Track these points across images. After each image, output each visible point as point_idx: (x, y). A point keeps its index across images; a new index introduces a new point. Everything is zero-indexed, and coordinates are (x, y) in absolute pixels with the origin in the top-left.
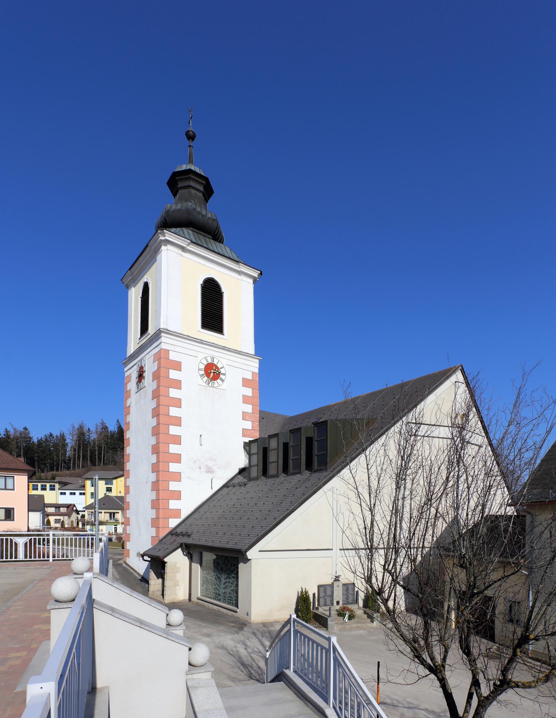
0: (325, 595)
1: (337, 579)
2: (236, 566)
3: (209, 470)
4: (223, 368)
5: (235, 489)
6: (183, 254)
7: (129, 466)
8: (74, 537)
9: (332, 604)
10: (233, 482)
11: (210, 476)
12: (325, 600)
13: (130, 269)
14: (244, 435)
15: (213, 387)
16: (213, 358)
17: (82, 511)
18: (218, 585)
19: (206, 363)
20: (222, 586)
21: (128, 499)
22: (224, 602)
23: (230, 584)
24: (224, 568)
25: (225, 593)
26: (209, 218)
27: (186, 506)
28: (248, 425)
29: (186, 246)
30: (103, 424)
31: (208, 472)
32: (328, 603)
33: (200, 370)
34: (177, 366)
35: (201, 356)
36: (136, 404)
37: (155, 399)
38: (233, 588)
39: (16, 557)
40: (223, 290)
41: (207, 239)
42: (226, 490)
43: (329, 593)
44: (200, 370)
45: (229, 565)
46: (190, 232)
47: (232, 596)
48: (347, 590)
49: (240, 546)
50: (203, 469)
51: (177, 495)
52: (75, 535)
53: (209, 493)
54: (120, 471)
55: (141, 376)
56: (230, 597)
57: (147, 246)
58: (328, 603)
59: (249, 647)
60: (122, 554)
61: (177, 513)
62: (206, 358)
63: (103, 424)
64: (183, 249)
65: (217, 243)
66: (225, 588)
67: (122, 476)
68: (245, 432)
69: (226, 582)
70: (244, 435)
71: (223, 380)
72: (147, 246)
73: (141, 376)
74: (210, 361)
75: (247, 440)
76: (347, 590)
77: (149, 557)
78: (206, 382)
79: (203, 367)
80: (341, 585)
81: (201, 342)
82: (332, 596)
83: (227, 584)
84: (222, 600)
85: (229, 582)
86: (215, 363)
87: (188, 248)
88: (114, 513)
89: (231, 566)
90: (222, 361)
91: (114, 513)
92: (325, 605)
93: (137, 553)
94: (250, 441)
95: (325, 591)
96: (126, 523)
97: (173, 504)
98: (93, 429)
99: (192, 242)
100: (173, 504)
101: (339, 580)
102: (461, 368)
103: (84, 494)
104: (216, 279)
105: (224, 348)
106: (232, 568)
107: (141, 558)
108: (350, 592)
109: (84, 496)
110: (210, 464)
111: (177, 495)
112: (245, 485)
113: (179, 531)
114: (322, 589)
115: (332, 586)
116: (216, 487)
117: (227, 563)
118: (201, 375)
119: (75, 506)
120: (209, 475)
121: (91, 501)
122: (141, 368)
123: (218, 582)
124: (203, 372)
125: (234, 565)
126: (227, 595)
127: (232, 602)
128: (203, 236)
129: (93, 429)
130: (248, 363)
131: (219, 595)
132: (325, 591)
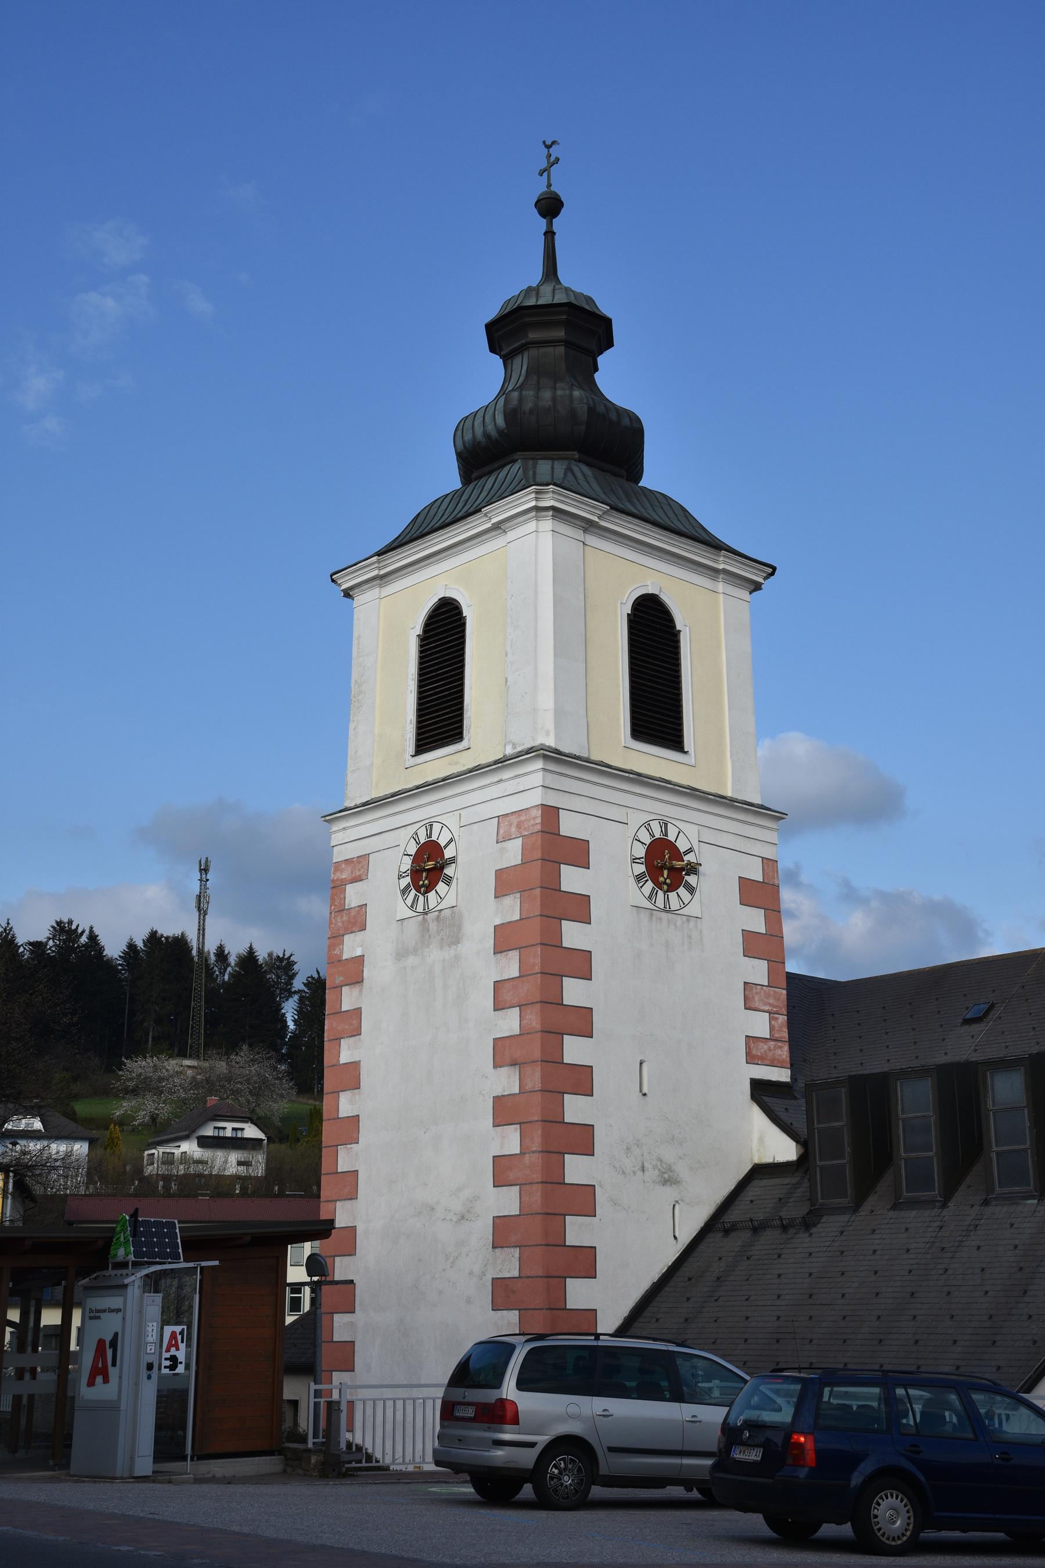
3: (668, 1179)
4: (690, 850)
6: (511, 535)
11: (670, 1193)
28: (760, 1025)
29: (596, 519)
30: (251, 948)
33: (634, 860)
34: (579, 853)
35: (637, 819)
39: (91, 1318)
40: (680, 623)
42: (715, 1239)
50: (652, 1174)
53: (671, 1253)
62: (647, 825)
63: (251, 948)
64: (588, 526)
71: (691, 890)
78: (650, 898)
79: (640, 852)
86: (671, 837)
87: (603, 523)
90: (689, 830)
99: (612, 508)
104: (665, 598)
105: (694, 793)
110: (669, 1155)
116: (687, 1232)
130: (751, 831)
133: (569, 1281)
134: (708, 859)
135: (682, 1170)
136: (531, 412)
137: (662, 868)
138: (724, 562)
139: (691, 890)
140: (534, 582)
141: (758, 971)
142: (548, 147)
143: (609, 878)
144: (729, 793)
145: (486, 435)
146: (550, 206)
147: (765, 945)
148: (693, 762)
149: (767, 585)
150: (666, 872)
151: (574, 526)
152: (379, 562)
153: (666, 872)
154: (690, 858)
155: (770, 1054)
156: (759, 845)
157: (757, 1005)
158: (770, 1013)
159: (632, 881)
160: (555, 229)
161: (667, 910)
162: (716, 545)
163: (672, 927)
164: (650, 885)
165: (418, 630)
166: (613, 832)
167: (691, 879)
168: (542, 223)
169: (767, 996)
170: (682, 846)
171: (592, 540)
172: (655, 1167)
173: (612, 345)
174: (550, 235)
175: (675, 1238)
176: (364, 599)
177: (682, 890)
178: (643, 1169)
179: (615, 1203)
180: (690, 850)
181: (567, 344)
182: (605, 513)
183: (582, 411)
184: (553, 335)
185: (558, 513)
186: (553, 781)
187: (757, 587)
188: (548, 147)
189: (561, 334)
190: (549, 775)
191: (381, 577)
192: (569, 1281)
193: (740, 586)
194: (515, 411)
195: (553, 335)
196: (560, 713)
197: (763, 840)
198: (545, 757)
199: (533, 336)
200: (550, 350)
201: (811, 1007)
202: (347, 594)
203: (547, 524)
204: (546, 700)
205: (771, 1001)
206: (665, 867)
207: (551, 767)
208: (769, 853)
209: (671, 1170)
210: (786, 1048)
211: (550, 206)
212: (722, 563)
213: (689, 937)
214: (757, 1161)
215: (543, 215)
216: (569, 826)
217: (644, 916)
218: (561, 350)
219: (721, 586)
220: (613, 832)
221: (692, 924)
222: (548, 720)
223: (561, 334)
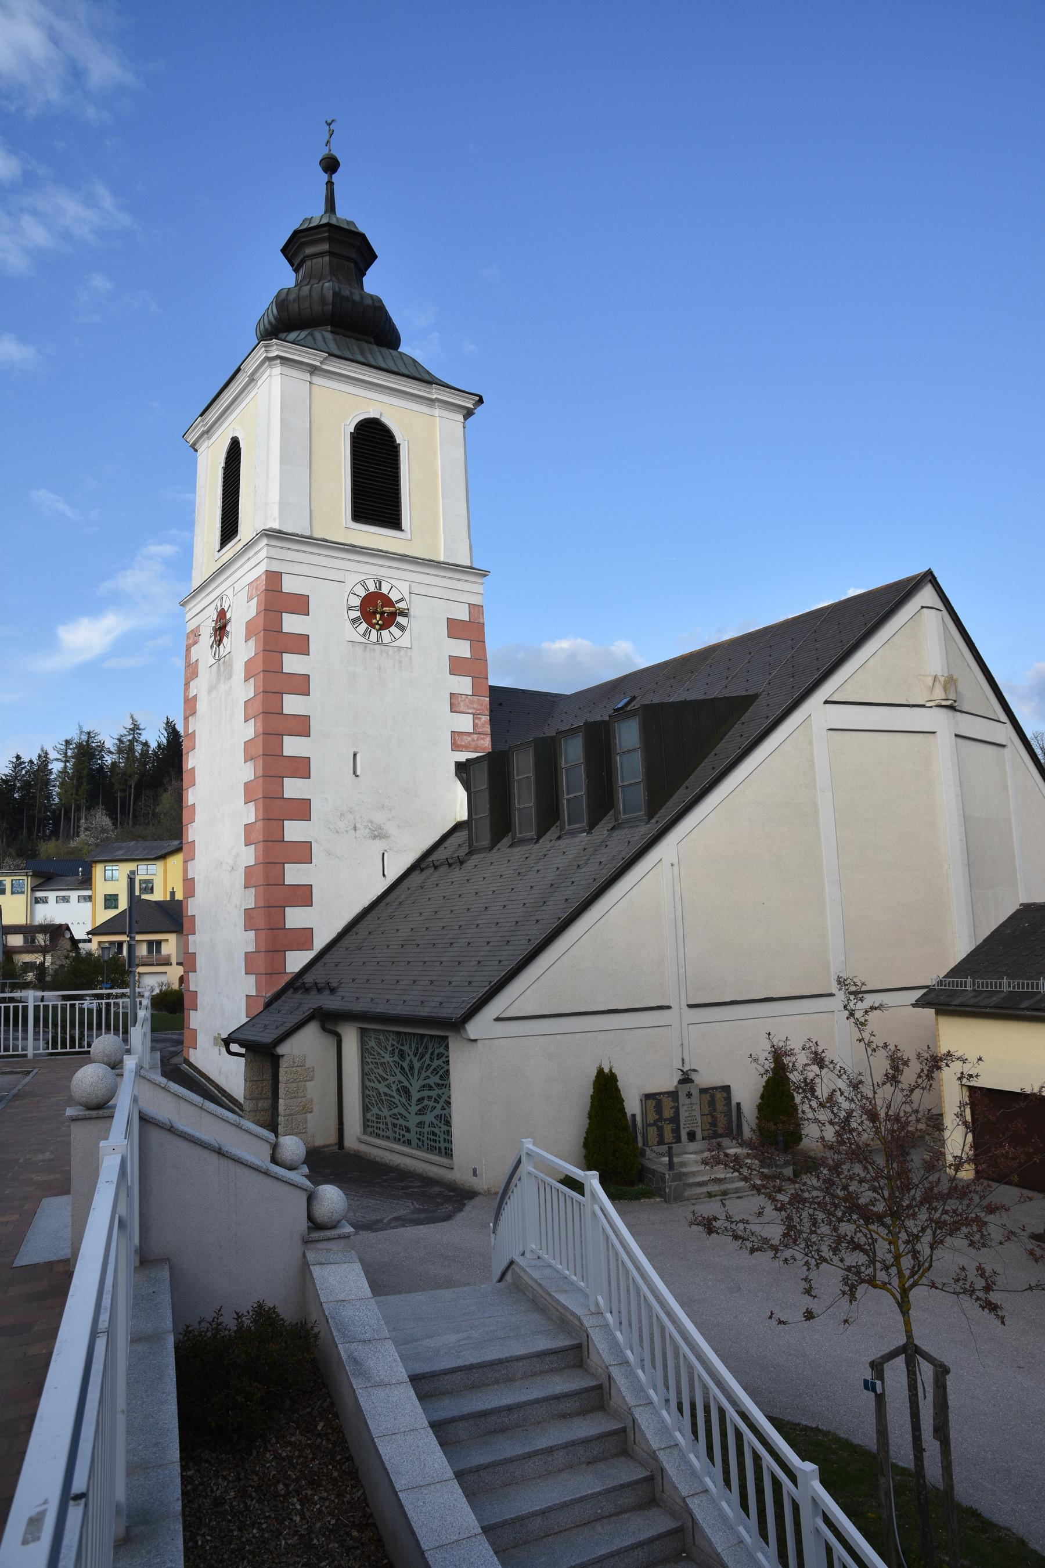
0: (660, 1119)
1: (686, 1079)
2: (444, 1059)
3: (378, 834)
5: (437, 874)
7: (194, 832)
8: (60, 1003)
9: (678, 1140)
10: (434, 857)
11: (379, 845)
12: (660, 1130)
13: (201, 415)
14: (455, 747)
15: (382, 644)
16: (380, 582)
17: (84, 941)
18: (404, 1106)
19: (363, 593)
20: (414, 1108)
21: (193, 908)
22: (418, 1148)
23: (432, 1103)
24: (417, 1065)
25: (420, 1124)
26: (368, 306)
27: (324, 920)
28: (465, 723)
31: (375, 837)
32: (668, 1136)
33: (350, 608)
34: (300, 605)
35: (352, 579)
36: (210, 691)
37: (252, 680)
38: (438, 1111)
41: (364, 345)
42: (416, 877)
43: (667, 1113)
44: (350, 608)
45: (427, 1057)
46: (329, 336)
47: (437, 1130)
48: (712, 1103)
49: (450, 1011)
50: (362, 832)
51: (304, 896)
52: (65, 998)
53: (381, 886)
54: (175, 839)
55: (221, 630)
56: (434, 1134)
57: (238, 370)
58: (668, 1136)
59: (715, 1219)
60: (181, 1042)
61: (303, 938)
62: (363, 584)
64: (313, 370)
65: (384, 350)
66: (421, 1112)
67: (179, 850)
68: (457, 741)
69: (423, 1098)
70: (455, 747)
72: (238, 370)
73: (221, 630)
74: (372, 589)
75: (463, 757)
76: (712, 1103)
77: (242, 1045)
78: (364, 635)
79: (356, 602)
80: (695, 1092)
81: (353, 549)
82: (675, 1120)
83: (426, 1102)
84: (415, 1141)
85: (430, 1097)
86: (385, 590)
87: (324, 367)
88: (159, 943)
89: (431, 1059)
90: (398, 586)
91: (159, 943)
92: (661, 1142)
93: (215, 1038)
94: (467, 760)
95: (658, 1109)
96: (188, 962)
97: (295, 918)
98: (110, 744)
100: (295, 918)
101: (691, 1081)
102: (930, 578)
103: (89, 898)
104: (386, 420)
105: (404, 558)
106: (436, 1063)
107: (223, 1050)
108: (720, 1106)
109: (89, 905)
110: (379, 818)
111: (304, 896)
112: (462, 863)
113: (308, 979)
114: (652, 1103)
115: (674, 1095)
116: (394, 871)
117: (418, 1042)
118: (354, 621)
119: (68, 928)
120: (377, 842)
121: (105, 915)
122: (222, 614)
123: (403, 1100)
124: (358, 614)
125: (440, 1056)
126: (426, 1129)
127: (437, 1145)
128: (356, 339)
129: (110, 744)
131: (408, 1130)
132: (658, 1109)
133: (4, 923)
134: (418, 607)
135: (391, 828)
136: (294, 300)
137: (375, 613)
138: (437, 393)
139: (402, 628)
140: (289, 418)
141: (464, 685)
142: (329, 125)
143: (329, 623)
144: (442, 560)
145: (270, 323)
146: (331, 165)
147: (472, 667)
148: (409, 537)
149: (479, 411)
150: (378, 616)
151: (301, 370)
152: (202, 421)
153: (378, 616)
154: (402, 605)
155: (473, 744)
156: (466, 594)
157: (462, 709)
158: (474, 714)
159: (348, 624)
160: (333, 180)
161: (379, 642)
162: (429, 381)
163: (385, 655)
164: (364, 625)
165: (223, 464)
166: (330, 591)
167: (400, 619)
168: (325, 177)
169: (472, 702)
170: (394, 596)
171: (318, 380)
172: (366, 827)
173: (375, 257)
174: (330, 184)
175: (384, 875)
176: (202, 448)
177: (393, 629)
178: (355, 829)
179: (329, 853)
180: (402, 600)
181: (330, 253)
182: (325, 359)
183: (329, 296)
184: (333, 251)
185: (284, 361)
186: (274, 553)
187: (468, 414)
188: (329, 125)
189: (325, 247)
190: (273, 550)
191: (207, 432)
192: (4, 923)
193: (454, 411)
194: (283, 301)
195: (333, 251)
196: (283, 505)
197: (471, 591)
198: (267, 535)
199: (309, 251)
200: (320, 260)
201: (508, 708)
202: (194, 448)
203: (277, 370)
204: (274, 496)
205: (475, 706)
206: (378, 611)
207: (274, 543)
208: (475, 600)
209: (380, 828)
210: (488, 739)
211: (331, 165)
212: (435, 393)
213: (400, 662)
214: (459, 820)
215: (326, 171)
216: (289, 585)
217: (359, 649)
218: (327, 259)
219: (437, 412)
220: (330, 591)
221: (402, 653)
222: (275, 510)
223: (325, 247)
